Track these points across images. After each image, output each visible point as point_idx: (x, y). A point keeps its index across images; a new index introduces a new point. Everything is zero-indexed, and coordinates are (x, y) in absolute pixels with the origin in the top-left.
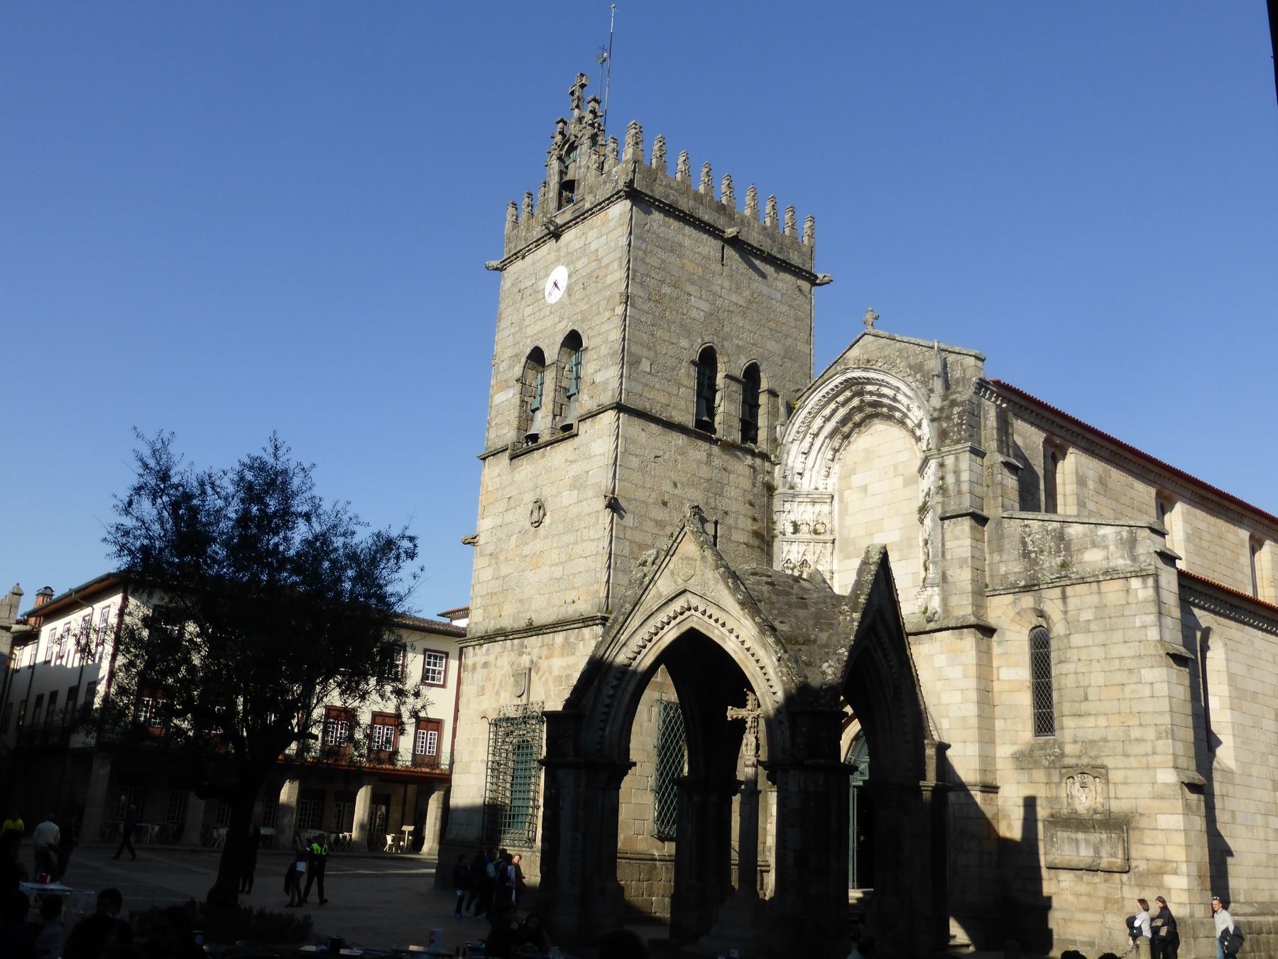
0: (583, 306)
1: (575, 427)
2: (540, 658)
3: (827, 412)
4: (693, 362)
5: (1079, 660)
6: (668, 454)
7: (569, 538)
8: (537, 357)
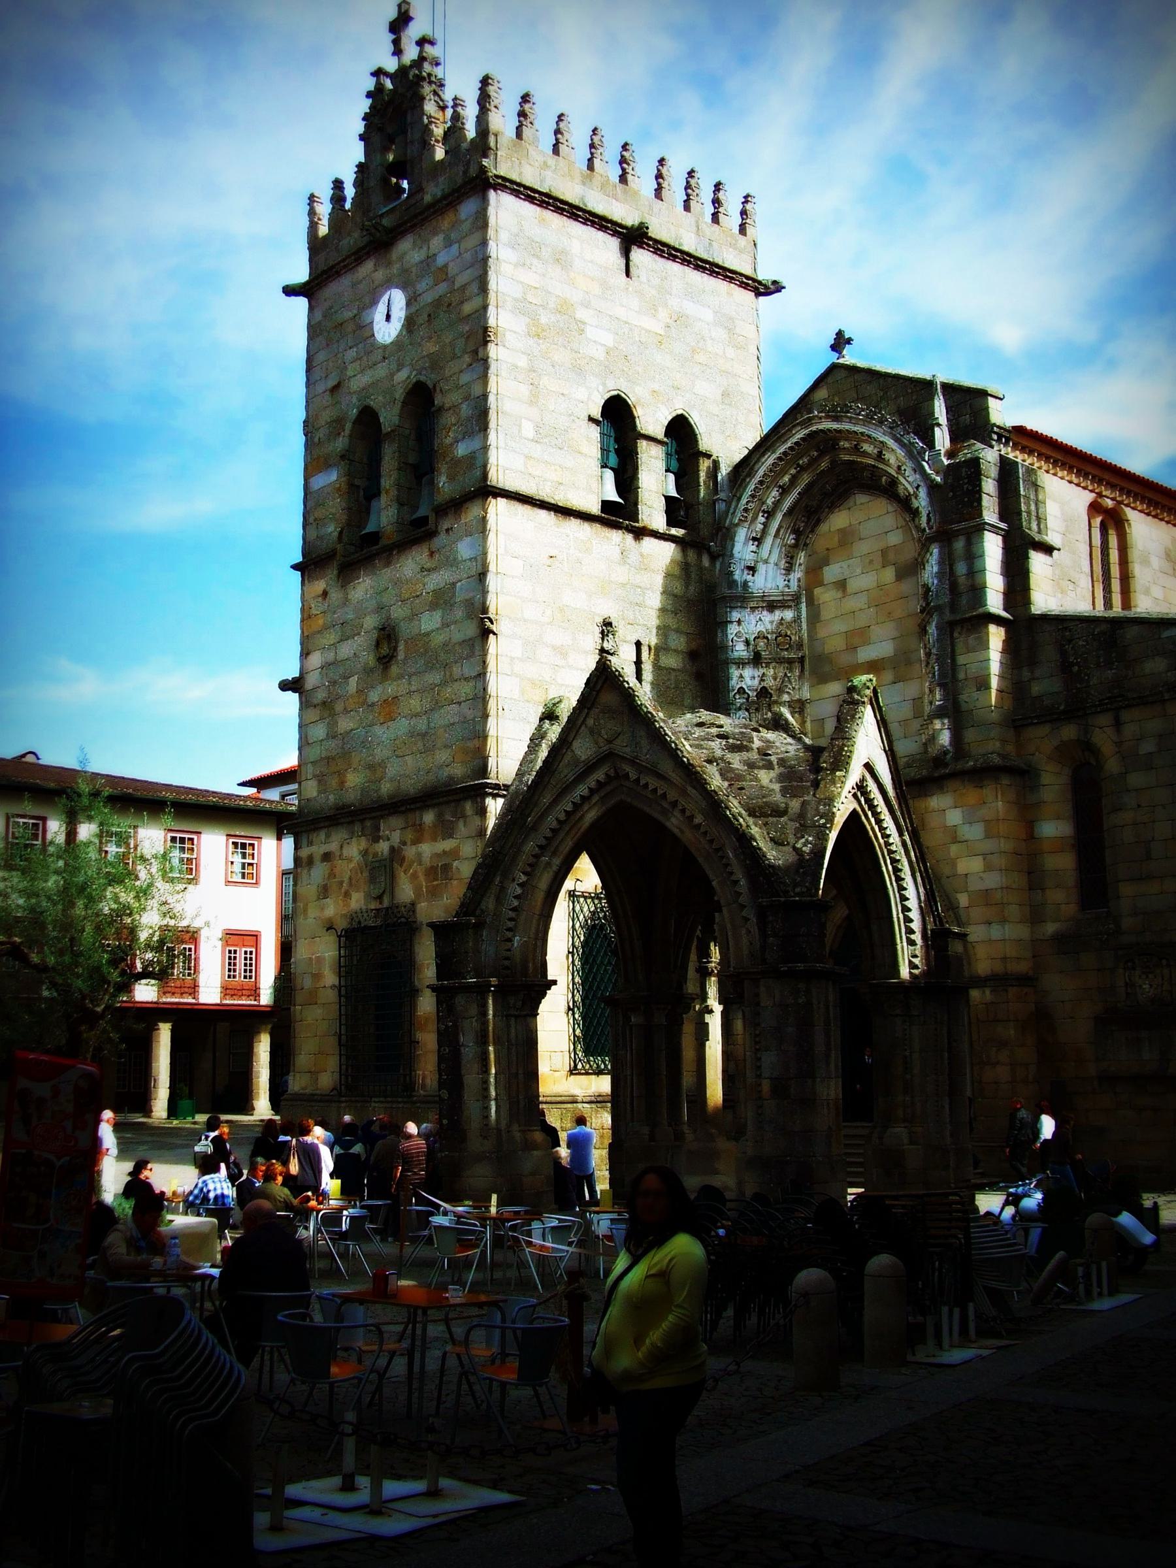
0: (431, 347)
1: (432, 519)
2: (404, 844)
5: (1139, 806)
7: (434, 677)
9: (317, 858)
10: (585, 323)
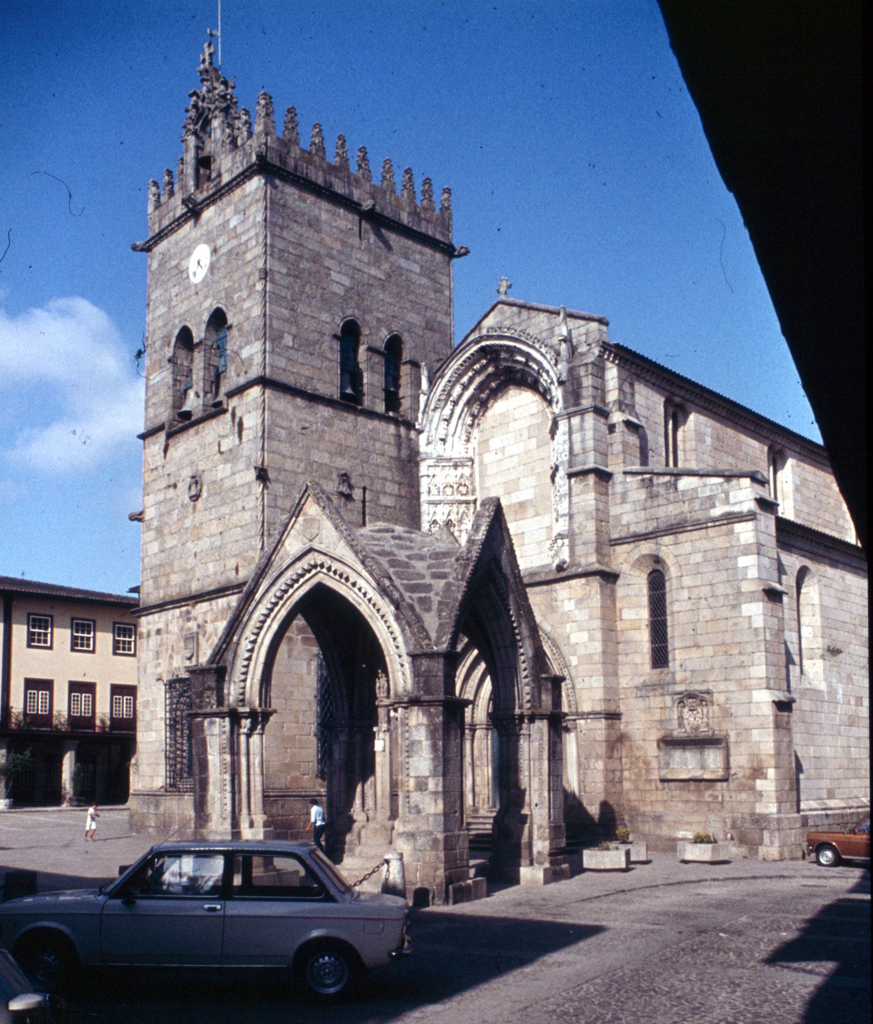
1: (225, 402)
3: (465, 379)
4: (335, 336)
6: (314, 427)
7: (225, 510)
8: (185, 336)
9: (153, 633)
10: (330, 269)
